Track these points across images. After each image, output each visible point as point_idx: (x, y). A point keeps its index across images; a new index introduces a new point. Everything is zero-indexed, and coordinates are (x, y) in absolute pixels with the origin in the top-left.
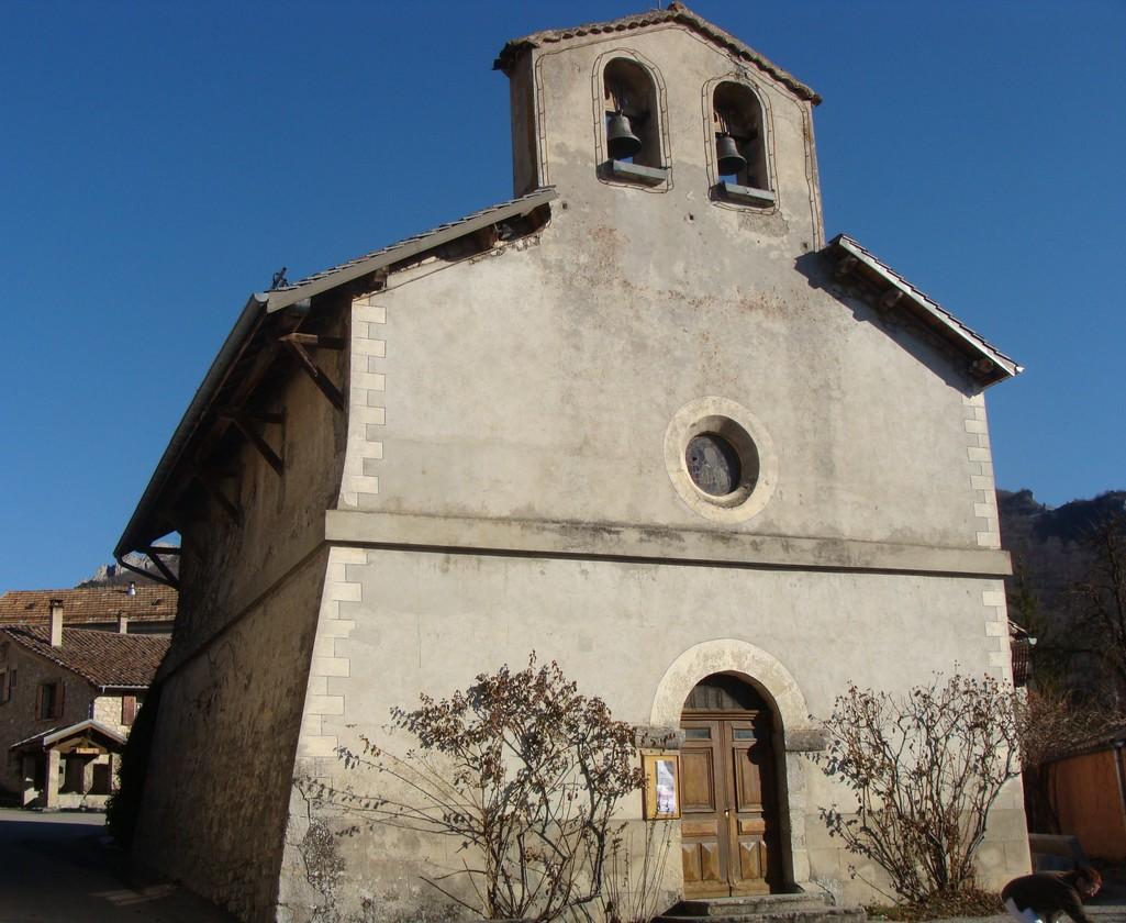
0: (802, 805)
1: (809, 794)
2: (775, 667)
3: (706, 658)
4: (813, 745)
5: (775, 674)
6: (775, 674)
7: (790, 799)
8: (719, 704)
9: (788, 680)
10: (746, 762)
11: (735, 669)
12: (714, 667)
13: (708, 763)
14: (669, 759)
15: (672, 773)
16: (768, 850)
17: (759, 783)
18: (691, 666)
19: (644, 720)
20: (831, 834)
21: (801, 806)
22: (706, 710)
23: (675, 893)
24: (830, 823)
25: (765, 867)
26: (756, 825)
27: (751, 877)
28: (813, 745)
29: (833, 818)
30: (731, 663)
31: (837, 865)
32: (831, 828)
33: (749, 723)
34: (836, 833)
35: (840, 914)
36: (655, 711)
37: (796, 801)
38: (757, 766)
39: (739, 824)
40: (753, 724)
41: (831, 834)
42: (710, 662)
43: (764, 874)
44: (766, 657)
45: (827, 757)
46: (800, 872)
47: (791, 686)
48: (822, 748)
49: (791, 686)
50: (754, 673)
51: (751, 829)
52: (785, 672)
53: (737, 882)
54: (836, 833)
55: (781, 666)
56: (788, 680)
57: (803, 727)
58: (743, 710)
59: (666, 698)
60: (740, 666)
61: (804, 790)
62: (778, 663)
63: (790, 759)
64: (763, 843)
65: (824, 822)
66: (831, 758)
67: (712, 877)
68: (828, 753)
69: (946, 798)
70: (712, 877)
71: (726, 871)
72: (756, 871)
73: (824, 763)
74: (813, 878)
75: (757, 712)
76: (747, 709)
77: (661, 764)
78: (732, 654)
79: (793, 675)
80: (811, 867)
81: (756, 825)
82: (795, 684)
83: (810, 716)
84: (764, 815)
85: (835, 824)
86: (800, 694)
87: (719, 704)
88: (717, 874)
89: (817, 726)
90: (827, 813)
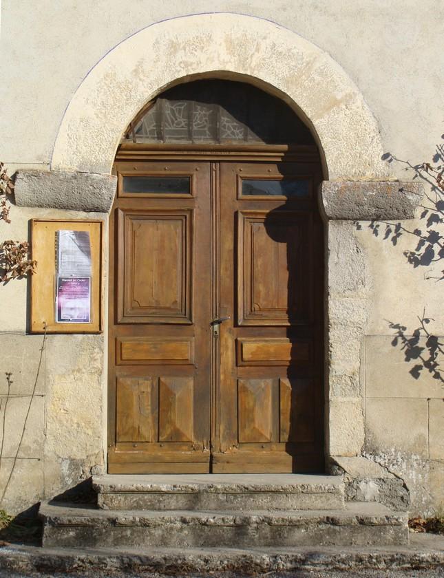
0: (359, 316)
1: (374, 298)
2: (317, 65)
3: (173, 47)
4: (385, 208)
5: (318, 78)
6: (318, 78)
7: (331, 303)
8: (215, 134)
9: (344, 86)
10: (263, 238)
11: (231, 68)
12: (187, 65)
13: (184, 238)
14: (81, 228)
15: (88, 253)
16: (294, 395)
17: (285, 275)
18: (140, 63)
19: (39, 158)
20: (415, 372)
21: (356, 318)
22: (211, 143)
23: (83, 463)
24: (413, 352)
25: (286, 424)
26: (272, 350)
27: (257, 441)
28: (385, 208)
29: (422, 343)
30: (225, 56)
31: (424, 431)
32: (414, 362)
33: (274, 172)
34: (424, 372)
35: (348, 525)
36: (62, 142)
37: (343, 308)
38: (283, 247)
39: (238, 346)
40: (281, 171)
41: (415, 372)
42: (180, 57)
43: (285, 437)
44: (302, 47)
45: (417, 232)
46: (342, 436)
47: (349, 99)
48: (406, 214)
49: (349, 99)
50: (271, 75)
51: (262, 357)
52: (338, 73)
53: (226, 449)
54: (424, 372)
55: (331, 61)
56: (344, 86)
57: (369, 174)
58: (262, 145)
59: (85, 121)
60: (243, 62)
61: (364, 291)
62: (325, 59)
63: (336, 235)
64: (286, 382)
65: (400, 350)
66: (425, 234)
67: (176, 439)
68: (422, 225)
69: (130, 350)
70: (176, 439)
71: (205, 430)
72: (267, 430)
73: (409, 243)
74: (370, 449)
75: (285, 147)
76: (268, 142)
77: (67, 237)
78: (229, 42)
79: (356, 80)
80: (367, 431)
81: (272, 350)
82: (360, 97)
83: (385, 156)
84: (291, 333)
85: (426, 355)
86: (367, 115)
87: (215, 134)
88: (190, 434)
89: (399, 173)
90: (409, 333)
